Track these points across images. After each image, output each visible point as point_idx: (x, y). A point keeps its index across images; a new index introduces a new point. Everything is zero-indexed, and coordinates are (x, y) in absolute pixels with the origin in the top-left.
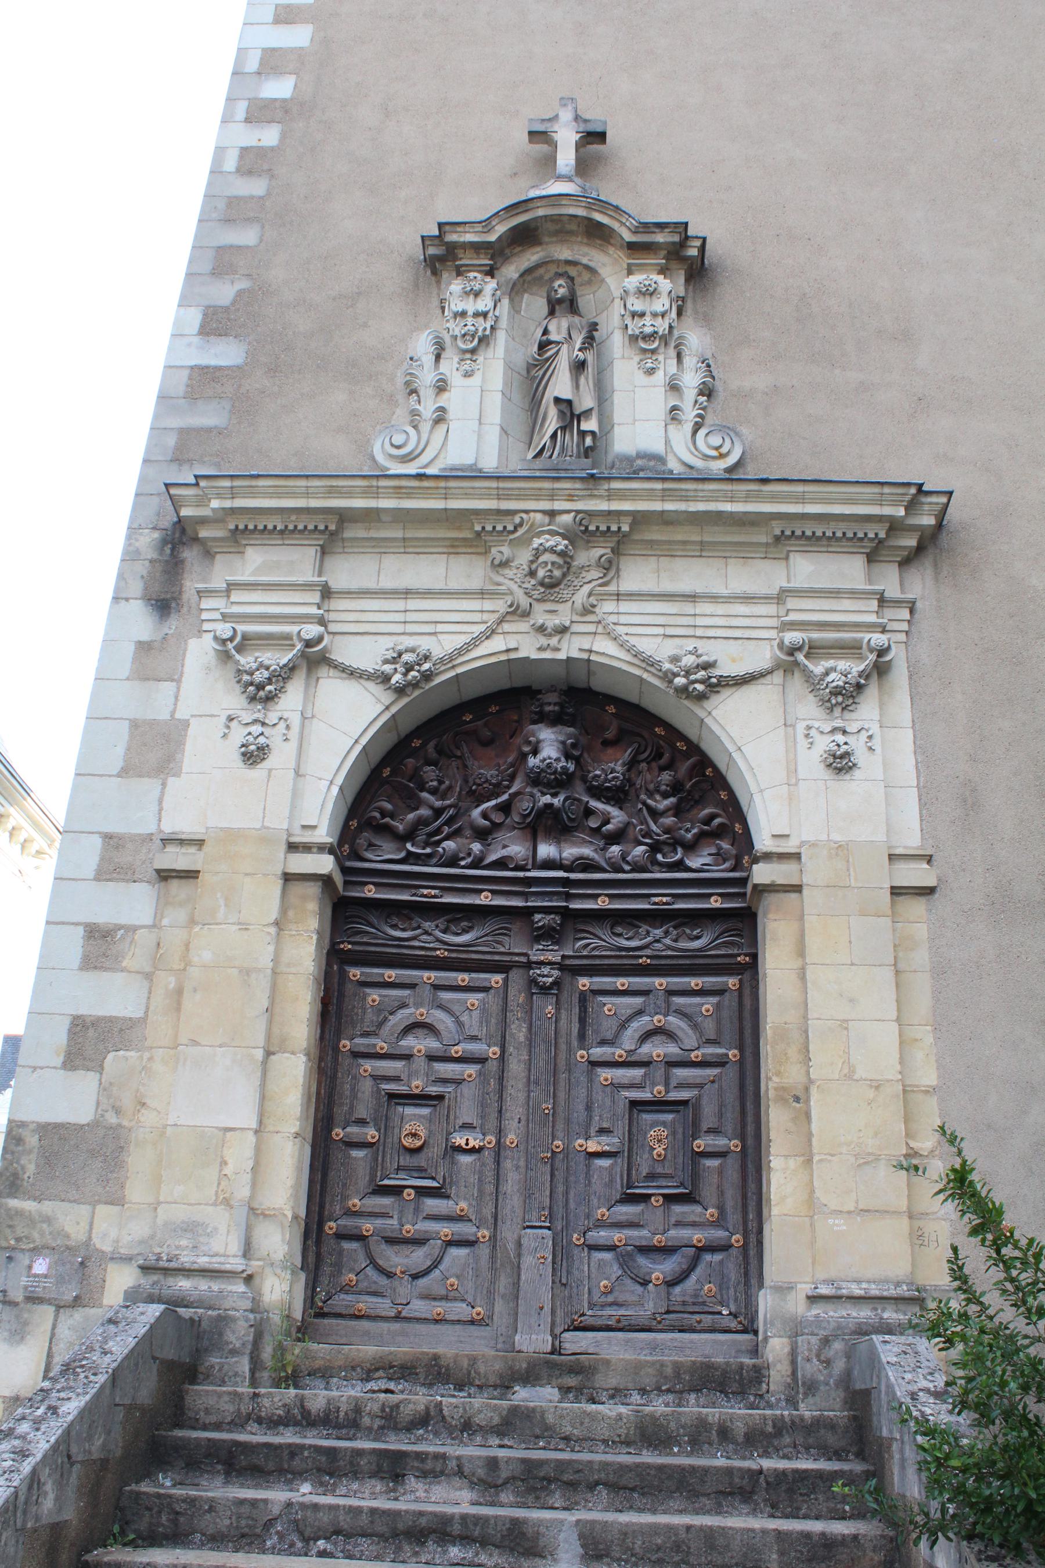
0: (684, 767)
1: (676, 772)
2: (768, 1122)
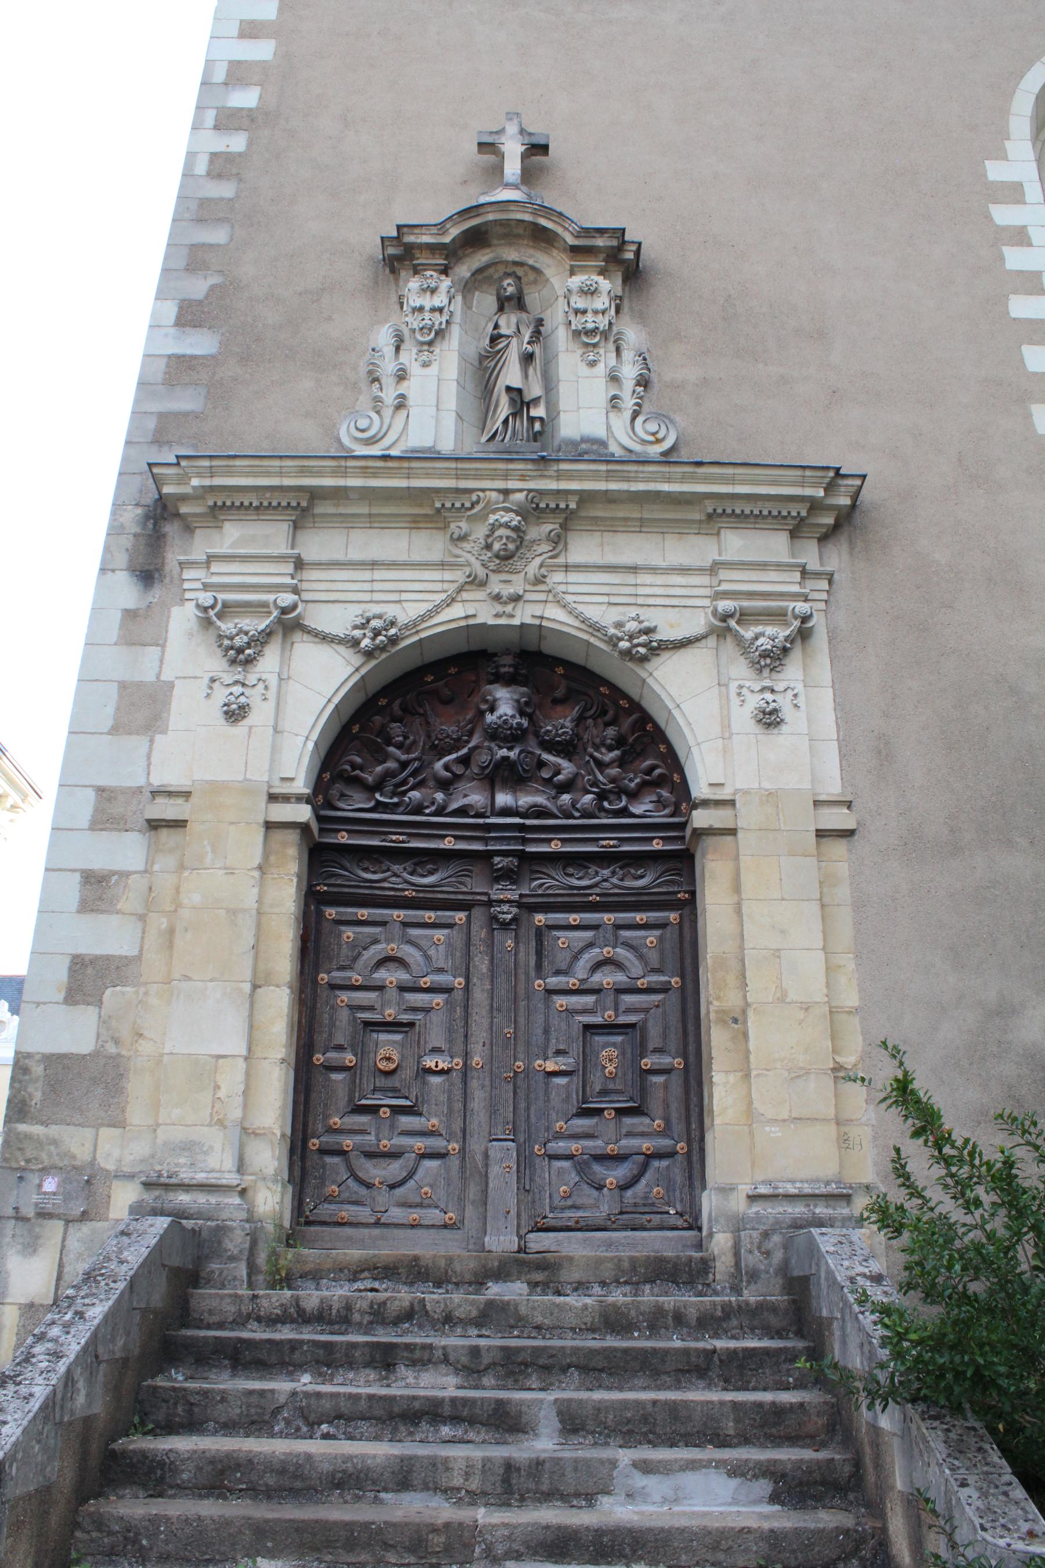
0: (627, 723)
1: (619, 727)
2: (710, 1041)
